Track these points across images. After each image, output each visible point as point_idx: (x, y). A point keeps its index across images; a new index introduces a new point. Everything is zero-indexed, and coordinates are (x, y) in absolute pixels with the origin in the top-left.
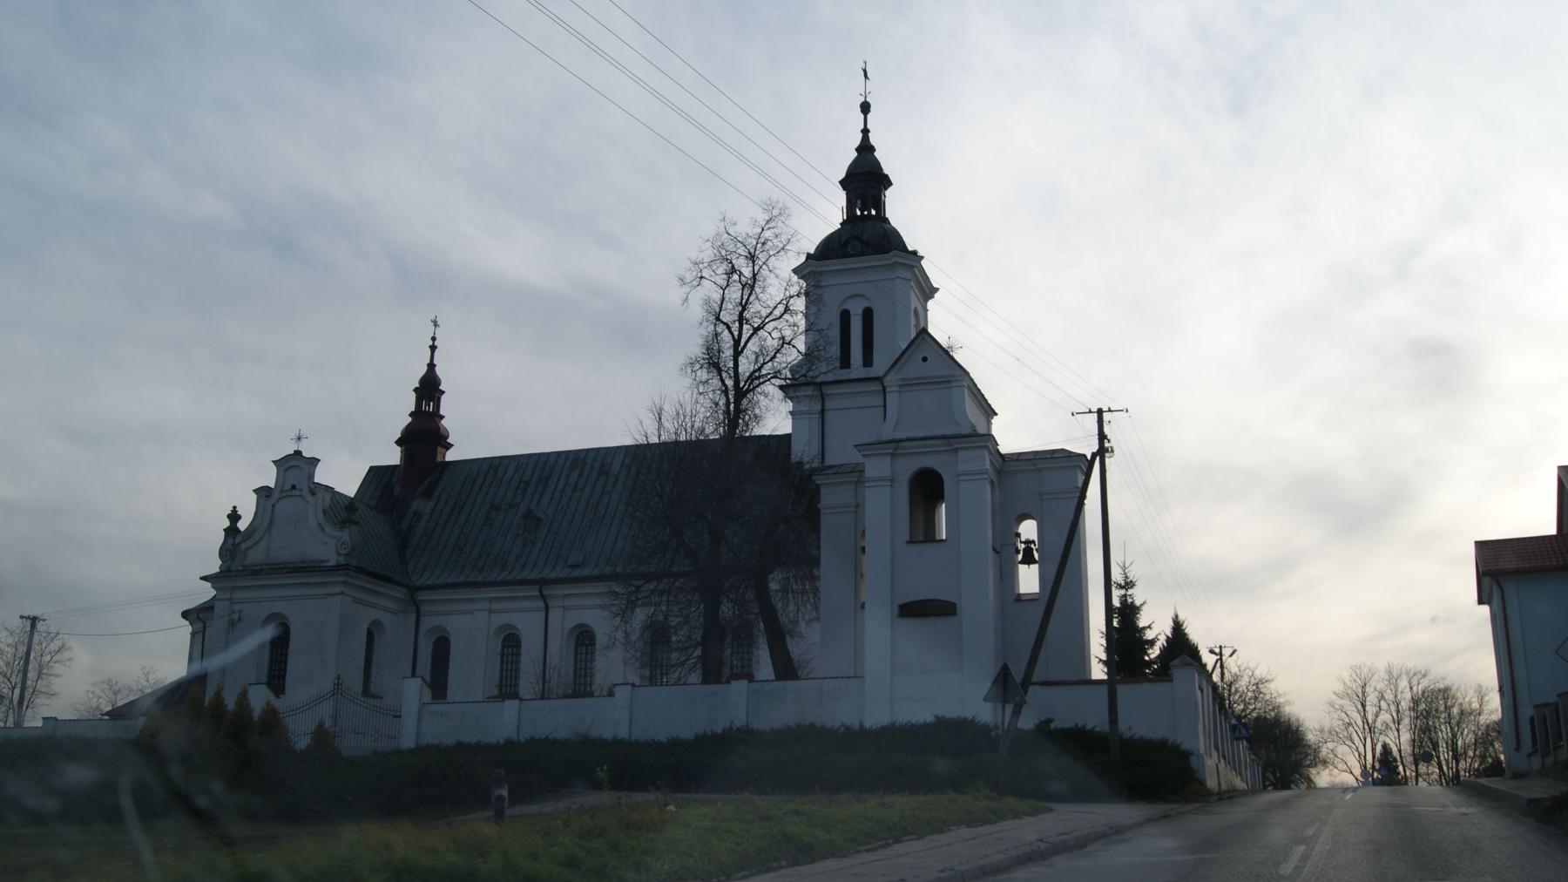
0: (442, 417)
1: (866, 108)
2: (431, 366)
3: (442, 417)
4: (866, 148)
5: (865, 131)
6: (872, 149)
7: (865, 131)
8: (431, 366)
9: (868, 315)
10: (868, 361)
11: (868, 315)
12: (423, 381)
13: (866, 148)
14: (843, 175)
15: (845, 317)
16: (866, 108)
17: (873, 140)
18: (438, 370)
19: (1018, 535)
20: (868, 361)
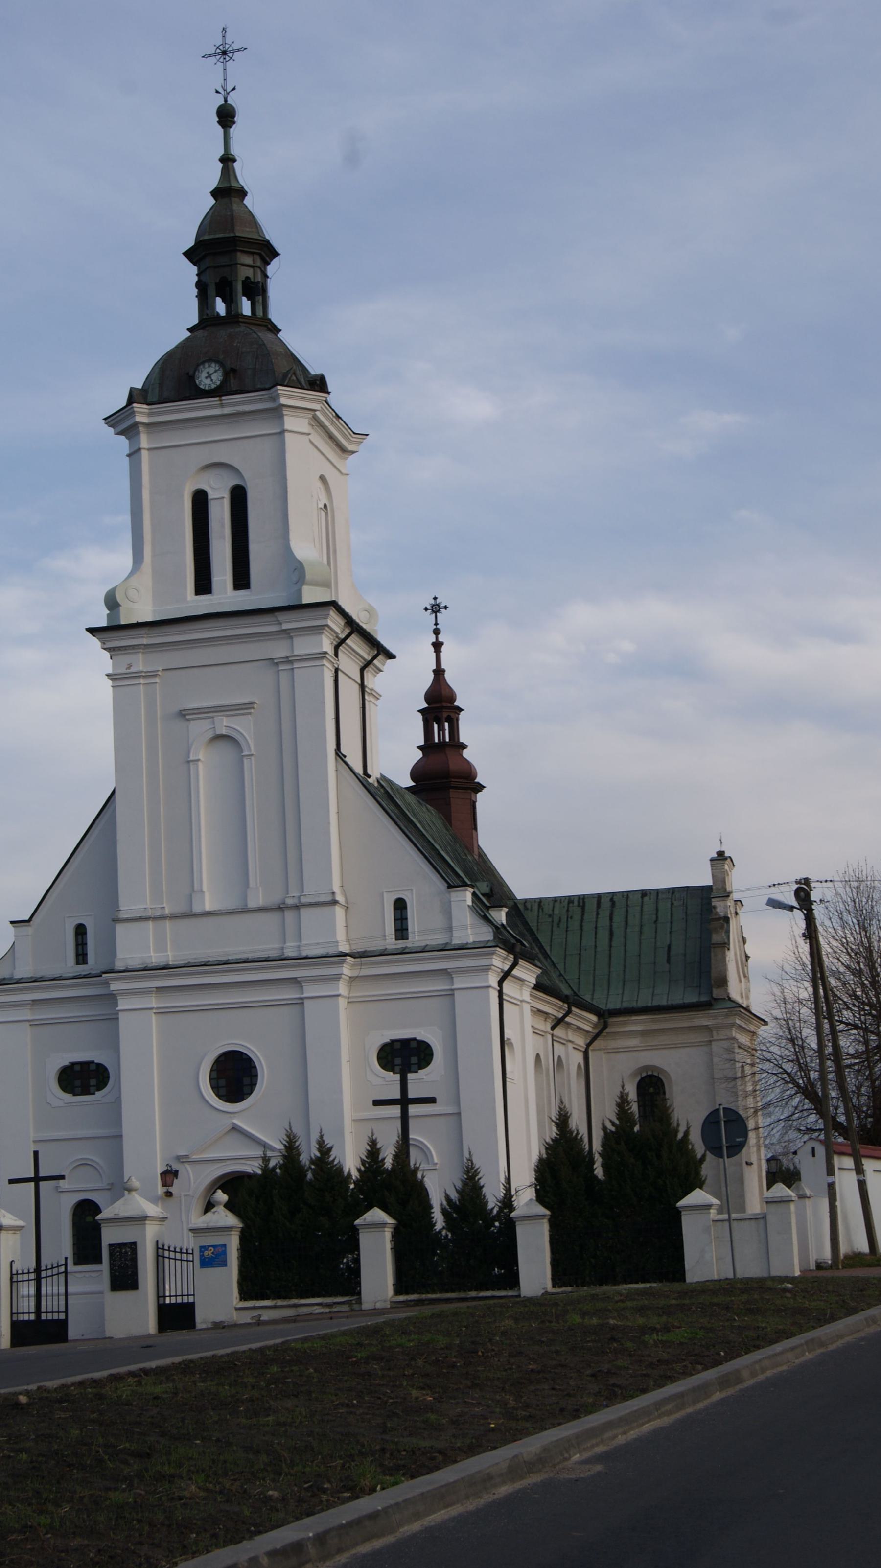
0: (463, 746)
1: (226, 116)
2: (439, 672)
3: (463, 746)
4: (228, 192)
5: (227, 160)
6: (242, 193)
7: (227, 160)
8: (439, 672)
9: (239, 498)
10: (241, 580)
11: (239, 498)
12: (430, 696)
13: (228, 192)
14: (190, 242)
15: (200, 501)
16: (226, 116)
17: (244, 175)
18: (449, 677)
19: (800, 909)
20: (241, 580)
